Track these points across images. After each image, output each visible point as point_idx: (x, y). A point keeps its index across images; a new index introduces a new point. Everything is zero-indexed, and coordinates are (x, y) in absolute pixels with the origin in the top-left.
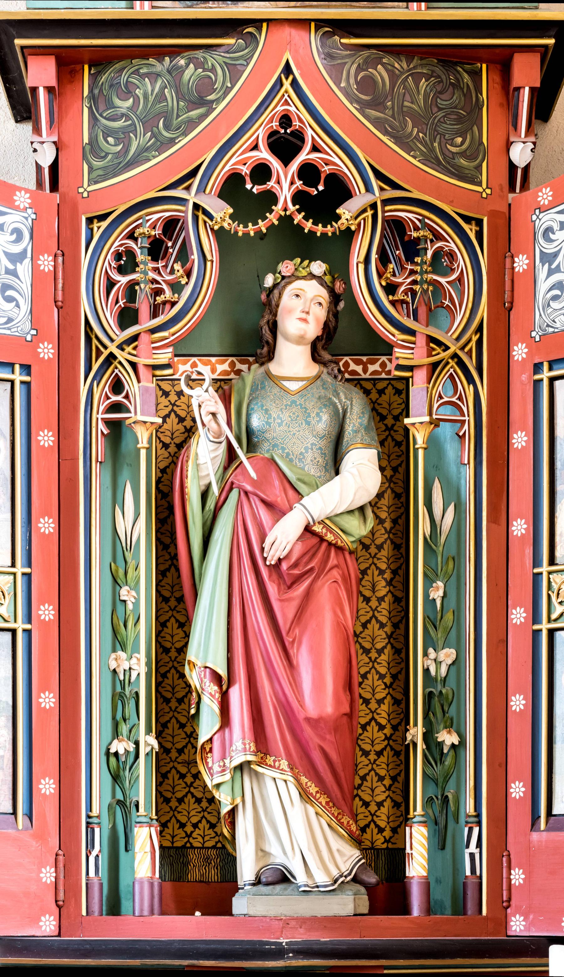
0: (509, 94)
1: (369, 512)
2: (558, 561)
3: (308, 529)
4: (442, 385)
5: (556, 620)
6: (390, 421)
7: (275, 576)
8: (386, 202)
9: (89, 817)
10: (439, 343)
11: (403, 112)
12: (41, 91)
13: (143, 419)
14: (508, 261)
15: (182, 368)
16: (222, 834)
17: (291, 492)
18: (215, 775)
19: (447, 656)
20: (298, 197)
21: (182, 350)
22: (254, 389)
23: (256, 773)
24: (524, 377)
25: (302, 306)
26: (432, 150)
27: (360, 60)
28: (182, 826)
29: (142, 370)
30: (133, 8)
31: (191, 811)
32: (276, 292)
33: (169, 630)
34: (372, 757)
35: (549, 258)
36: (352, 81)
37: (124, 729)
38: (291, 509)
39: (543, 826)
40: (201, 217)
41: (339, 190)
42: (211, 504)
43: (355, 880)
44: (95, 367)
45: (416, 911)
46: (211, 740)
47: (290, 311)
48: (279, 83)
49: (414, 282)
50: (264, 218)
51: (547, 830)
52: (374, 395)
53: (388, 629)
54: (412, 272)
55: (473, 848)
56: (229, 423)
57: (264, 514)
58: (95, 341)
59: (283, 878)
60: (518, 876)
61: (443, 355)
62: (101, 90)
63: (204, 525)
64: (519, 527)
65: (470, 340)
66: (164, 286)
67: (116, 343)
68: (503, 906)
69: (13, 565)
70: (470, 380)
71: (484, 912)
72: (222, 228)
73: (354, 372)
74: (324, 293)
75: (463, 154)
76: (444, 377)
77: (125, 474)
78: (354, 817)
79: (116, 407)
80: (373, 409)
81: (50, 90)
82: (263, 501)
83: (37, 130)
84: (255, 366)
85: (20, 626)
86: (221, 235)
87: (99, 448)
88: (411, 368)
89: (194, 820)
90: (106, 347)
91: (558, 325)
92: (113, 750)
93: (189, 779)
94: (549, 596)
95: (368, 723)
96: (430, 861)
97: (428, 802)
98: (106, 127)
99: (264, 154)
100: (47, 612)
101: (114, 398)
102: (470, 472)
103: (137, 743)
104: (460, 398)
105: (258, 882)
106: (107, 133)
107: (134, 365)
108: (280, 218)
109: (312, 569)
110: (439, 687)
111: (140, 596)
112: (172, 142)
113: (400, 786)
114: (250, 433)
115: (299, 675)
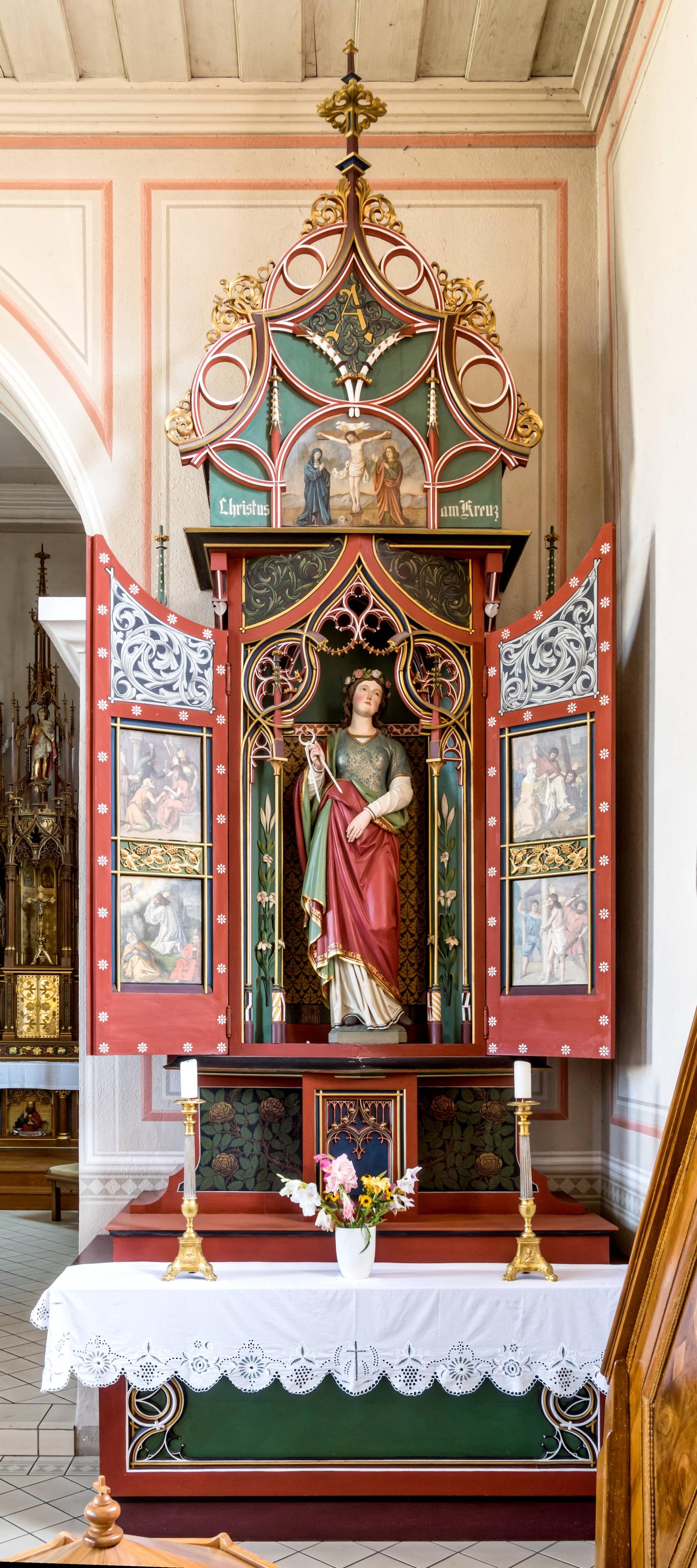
0: (484, 577)
1: (406, 813)
2: (515, 841)
3: (372, 822)
4: (447, 741)
5: (514, 875)
6: (416, 761)
7: (353, 848)
8: (415, 637)
9: (245, 986)
10: (446, 717)
11: (425, 586)
12: (219, 572)
13: (277, 760)
14: (485, 670)
15: (297, 730)
16: (321, 996)
17: (362, 801)
18: (318, 963)
19: (451, 894)
20: (365, 634)
21: (299, 719)
22: (340, 742)
23: (342, 961)
24: (494, 736)
25: (367, 694)
26: (441, 607)
27: (400, 557)
28: (298, 991)
29: (276, 731)
31: (303, 983)
32: (352, 687)
33: (290, 879)
34: (407, 952)
35: (508, 669)
36: (396, 568)
37: (266, 936)
38: (362, 810)
39: (507, 993)
40: (310, 644)
41: (388, 630)
42: (315, 807)
43: (399, 1023)
44: (249, 729)
45: (434, 1042)
46: (316, 942)
47: (360, 698)
48: (355, 569)
49: (431, 682)
50: (346, 645)
51: (510, 994)
52: (407, 746)
53: (416, 879)
54: (430, 676)
55: (467, 1005)
56: (326, 761)
57: (346, 813)
58: (249, 715)
59: (357, 1022)
60: (492, 1021)
61: (448, 723)
62: (252, 573)
63: (311, 819)
64: (492, 821)
65: (463, 715)
66: (289, 684)
67: (262, 716)
68: (484, 1036)
69: (202, 841)
70: (464, 738)
71: (473, 1042)
72: (322, 651)
73: (396, 733)
74: (379, 687)
75: (458, 610)
76: (449, 736)
77: (266, 789)
78: (397, 985)
79: (261, 752)
80: (408, 754)
81: (223, 572)
82: (346, 806)
83: (216, 595)
84: (340, 729)
85: (206, 876)
86: (321, 655)
87: (251, 775)
88: (429, 731)
89: (305, 988)
90: (255, 718)
91: (514, 707)
92: (259, 948)
93: (302, 965)
94: (510, 861)
95: (405, 933)
96: (443, 1012)
97: (441, 978)
98: (255, 593)
99: (346, 609)
100: (221, 869)
101: (260, 747)
102: (463, 790)
103: (273, 944)
104: (458, 748)
105: (343, 1024)
106: (256, 596)
107: (272, 728)
108: (355, 646)
109: (374, 845)
110: (447, 912)
111: (275, 860)
112: (293, 602)
113: (423, 969)
114: (338, 767)
115: (367, 905)
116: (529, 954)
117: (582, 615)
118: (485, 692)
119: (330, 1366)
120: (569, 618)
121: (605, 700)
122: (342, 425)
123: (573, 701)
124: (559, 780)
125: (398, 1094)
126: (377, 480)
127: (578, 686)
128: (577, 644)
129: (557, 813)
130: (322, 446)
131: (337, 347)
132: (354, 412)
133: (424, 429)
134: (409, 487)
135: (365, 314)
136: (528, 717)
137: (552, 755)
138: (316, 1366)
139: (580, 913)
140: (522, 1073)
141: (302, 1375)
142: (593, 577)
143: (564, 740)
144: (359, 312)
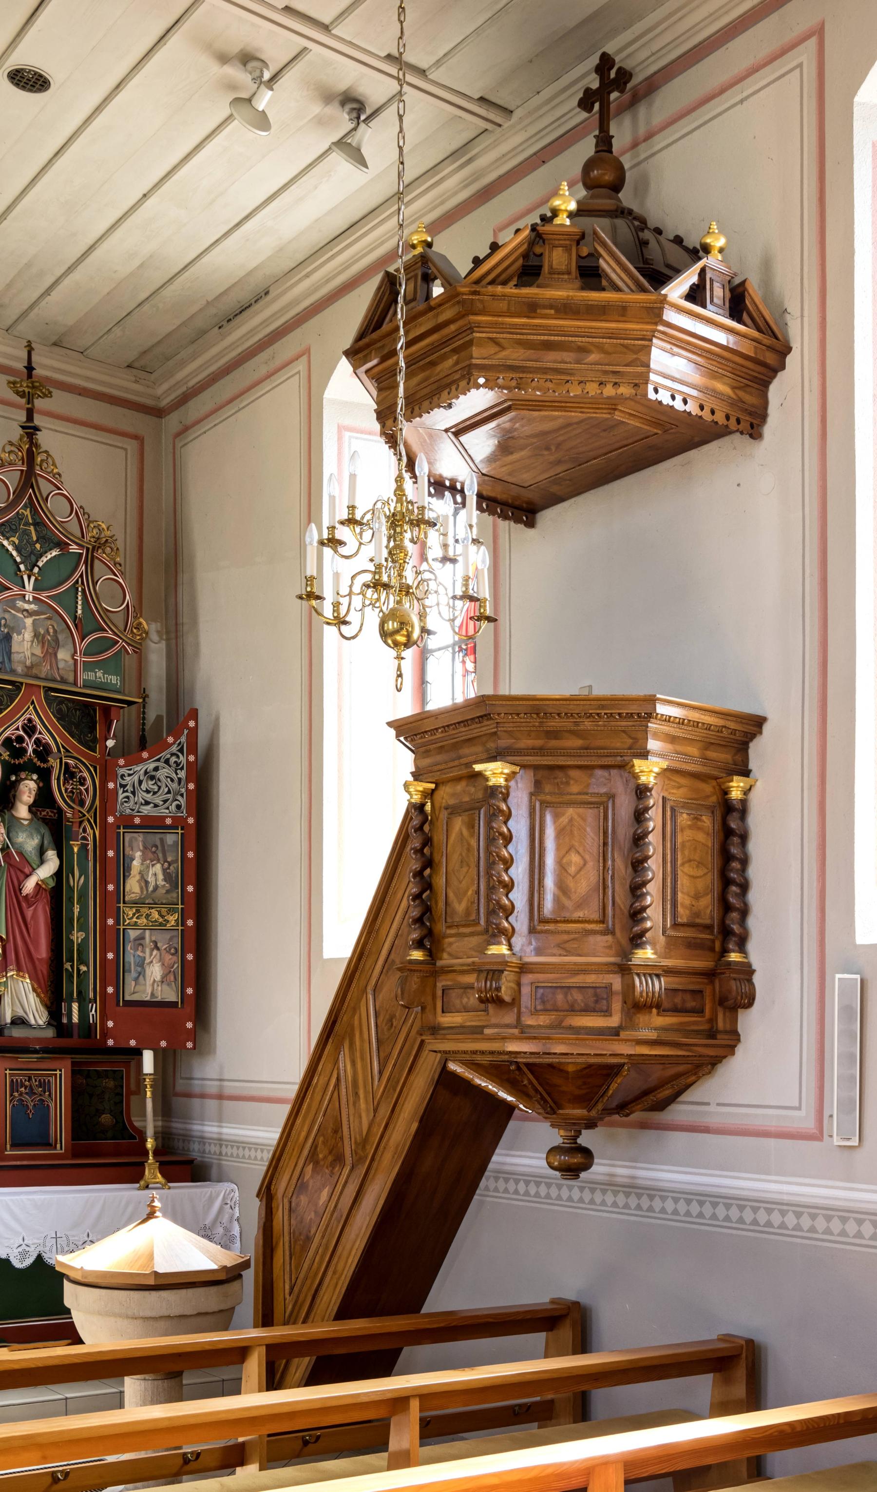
3: (37, 884)
20: (34, 751)
26: (80, 737)
30: (443, 1012)
35: (123, 786)
57: (22, 876)
60: (110, 1024)
64: (111, 887)
74: (36, 786)
75: (91, 741)
99: (22, 733)
116: (136, 979)
117: (176, 762)
118: (107, 800)
119: (41, 1249)
120: (167, 762)
121: (191, 820)
122: (20, 604)
123: (170, 817)
124: (158, 866)
125: (58, 1072)
126: (43, 647)
127: (173, 808)
128: (172, 780)
129: (156, 888)
130: (7, 616)
131: (17, 548)
132: (29, 597)
133: (75, 618)
134: (63, 655)
135: (36, 530)
136: (137, 821)
137: (154, 849)
138: (32, 1249)
139: (172, 954)
140: (148, 1057)
141: (24, 1255)
142: (183, 739)
143: (162, 840)
144: (32, 528)
